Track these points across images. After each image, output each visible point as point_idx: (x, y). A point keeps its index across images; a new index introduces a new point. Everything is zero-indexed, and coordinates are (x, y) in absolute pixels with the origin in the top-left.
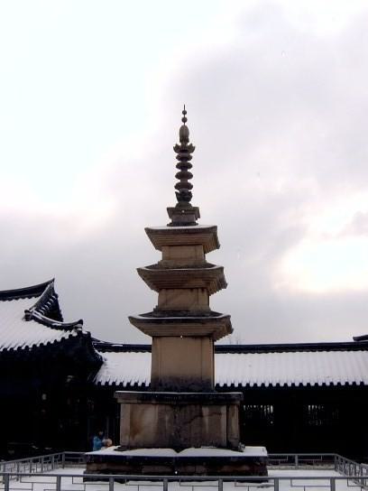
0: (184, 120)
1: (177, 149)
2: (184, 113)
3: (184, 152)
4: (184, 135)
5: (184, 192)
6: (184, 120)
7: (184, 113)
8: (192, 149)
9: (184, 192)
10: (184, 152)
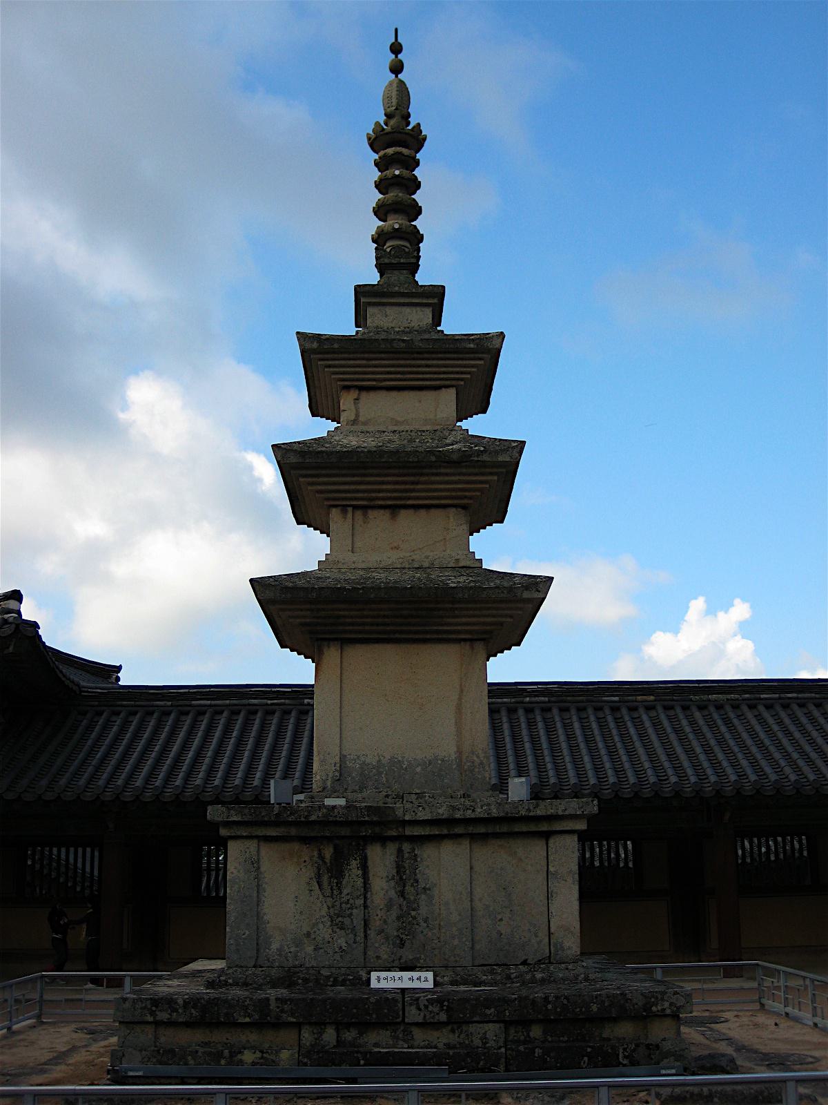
0: (397, 68)
2: (396, 48)
3: (397, 145)
4: (399, 102)
5: (398, 244)
6: (397, 68)
7: (396, 48)
8: (417, 139)
9: (398, 244)
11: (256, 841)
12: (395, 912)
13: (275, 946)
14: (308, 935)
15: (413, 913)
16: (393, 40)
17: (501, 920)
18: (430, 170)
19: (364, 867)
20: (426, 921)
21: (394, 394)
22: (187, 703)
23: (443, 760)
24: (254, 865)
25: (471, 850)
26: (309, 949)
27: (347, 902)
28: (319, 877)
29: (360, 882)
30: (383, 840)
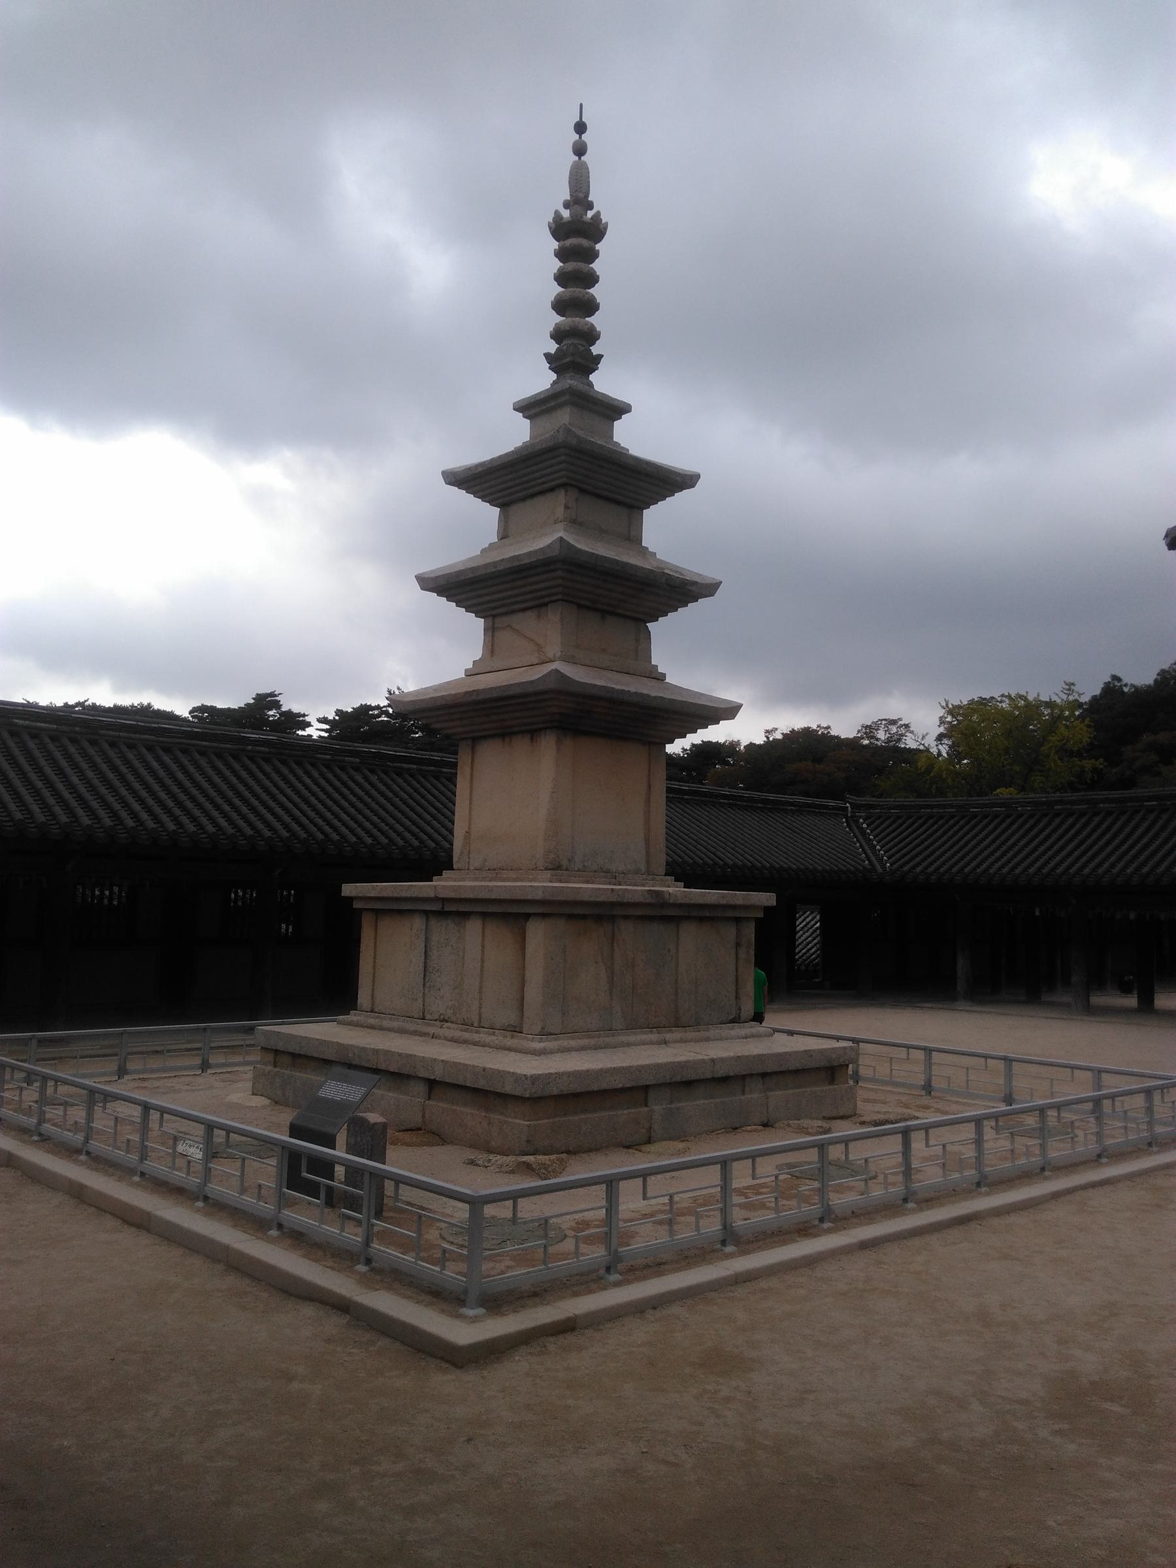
0: (580, 150)
1: (560, 229)
2: (580, 128)
3: (578, 235)
4: (579, 198)
5: (575, 352)
6: (580, 150)
7: (580, 128)
8: (596, 231)
9: (575, 352)
10: (578, 235)
11: (418, 922)
18: (608, 260)
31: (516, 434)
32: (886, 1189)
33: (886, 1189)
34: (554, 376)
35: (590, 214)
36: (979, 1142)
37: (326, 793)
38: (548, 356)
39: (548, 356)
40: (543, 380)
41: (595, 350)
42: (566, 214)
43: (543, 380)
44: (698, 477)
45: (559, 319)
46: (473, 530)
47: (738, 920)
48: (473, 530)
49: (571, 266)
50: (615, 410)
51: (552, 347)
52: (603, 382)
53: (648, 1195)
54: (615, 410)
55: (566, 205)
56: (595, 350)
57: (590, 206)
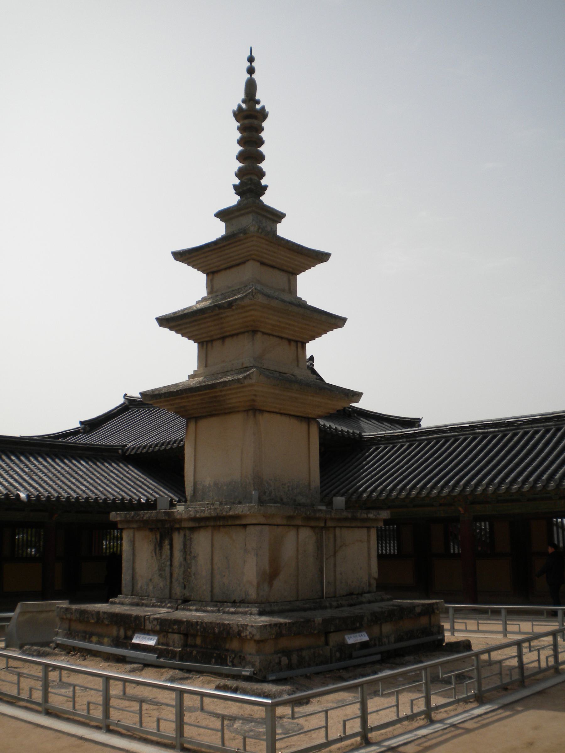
0: (251, 71)
1: (239, 114)
2: (251, 59)
3: (251, 119)
5: (250, 181)
6: (251, 71)
7: (251, 59)
8: (263, 115)
9: (250, 181)
10: (251, 119)
11: (132, 530)
12: (182, 569)
13: (139, 585)
14: (151, 580)
15: (189, 570)
16: (249, 54)
17: (224, 576)
18: (269, 131)
19: (171, 545)
20: (194, 574)
21: (228, 271)
22: (414, 439)
23: (235, 482)
24: (133, 542)
25: (212, 536)
26: (151, 587)
27: (164, 563)
28: (155, 549)
29: (169, 552)
30: (179, 529)
31: (217, 230)
32: (505, 636)
33: (505, 636)
34: (238, 198)
35: (258, 107)
36: (520, 656)
37: (121, 484)
38: (235, 187)
39: (235, 187)
40: (233, 200)
41: (264, 182)
42: (244, 106)
43: (233, 200)
44: (362, 394)
45: (241, 165)
46: (191, 288)
47: (369, 528)
48: (191, 288)
49: (246, 122)
50: (278, 216)
51: (237, 181)
52: (267, 199)
53: (295, 716)
54: (278, 216)
55: (244, 101)
56: (264, 182)
57: (258, 102)
